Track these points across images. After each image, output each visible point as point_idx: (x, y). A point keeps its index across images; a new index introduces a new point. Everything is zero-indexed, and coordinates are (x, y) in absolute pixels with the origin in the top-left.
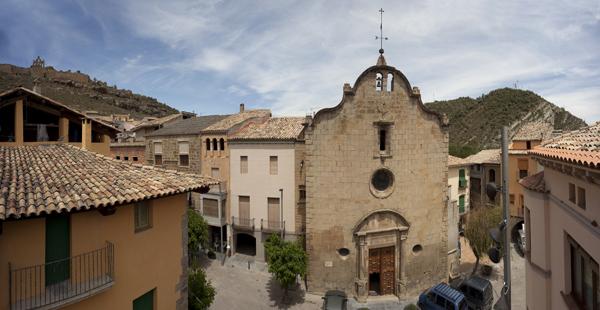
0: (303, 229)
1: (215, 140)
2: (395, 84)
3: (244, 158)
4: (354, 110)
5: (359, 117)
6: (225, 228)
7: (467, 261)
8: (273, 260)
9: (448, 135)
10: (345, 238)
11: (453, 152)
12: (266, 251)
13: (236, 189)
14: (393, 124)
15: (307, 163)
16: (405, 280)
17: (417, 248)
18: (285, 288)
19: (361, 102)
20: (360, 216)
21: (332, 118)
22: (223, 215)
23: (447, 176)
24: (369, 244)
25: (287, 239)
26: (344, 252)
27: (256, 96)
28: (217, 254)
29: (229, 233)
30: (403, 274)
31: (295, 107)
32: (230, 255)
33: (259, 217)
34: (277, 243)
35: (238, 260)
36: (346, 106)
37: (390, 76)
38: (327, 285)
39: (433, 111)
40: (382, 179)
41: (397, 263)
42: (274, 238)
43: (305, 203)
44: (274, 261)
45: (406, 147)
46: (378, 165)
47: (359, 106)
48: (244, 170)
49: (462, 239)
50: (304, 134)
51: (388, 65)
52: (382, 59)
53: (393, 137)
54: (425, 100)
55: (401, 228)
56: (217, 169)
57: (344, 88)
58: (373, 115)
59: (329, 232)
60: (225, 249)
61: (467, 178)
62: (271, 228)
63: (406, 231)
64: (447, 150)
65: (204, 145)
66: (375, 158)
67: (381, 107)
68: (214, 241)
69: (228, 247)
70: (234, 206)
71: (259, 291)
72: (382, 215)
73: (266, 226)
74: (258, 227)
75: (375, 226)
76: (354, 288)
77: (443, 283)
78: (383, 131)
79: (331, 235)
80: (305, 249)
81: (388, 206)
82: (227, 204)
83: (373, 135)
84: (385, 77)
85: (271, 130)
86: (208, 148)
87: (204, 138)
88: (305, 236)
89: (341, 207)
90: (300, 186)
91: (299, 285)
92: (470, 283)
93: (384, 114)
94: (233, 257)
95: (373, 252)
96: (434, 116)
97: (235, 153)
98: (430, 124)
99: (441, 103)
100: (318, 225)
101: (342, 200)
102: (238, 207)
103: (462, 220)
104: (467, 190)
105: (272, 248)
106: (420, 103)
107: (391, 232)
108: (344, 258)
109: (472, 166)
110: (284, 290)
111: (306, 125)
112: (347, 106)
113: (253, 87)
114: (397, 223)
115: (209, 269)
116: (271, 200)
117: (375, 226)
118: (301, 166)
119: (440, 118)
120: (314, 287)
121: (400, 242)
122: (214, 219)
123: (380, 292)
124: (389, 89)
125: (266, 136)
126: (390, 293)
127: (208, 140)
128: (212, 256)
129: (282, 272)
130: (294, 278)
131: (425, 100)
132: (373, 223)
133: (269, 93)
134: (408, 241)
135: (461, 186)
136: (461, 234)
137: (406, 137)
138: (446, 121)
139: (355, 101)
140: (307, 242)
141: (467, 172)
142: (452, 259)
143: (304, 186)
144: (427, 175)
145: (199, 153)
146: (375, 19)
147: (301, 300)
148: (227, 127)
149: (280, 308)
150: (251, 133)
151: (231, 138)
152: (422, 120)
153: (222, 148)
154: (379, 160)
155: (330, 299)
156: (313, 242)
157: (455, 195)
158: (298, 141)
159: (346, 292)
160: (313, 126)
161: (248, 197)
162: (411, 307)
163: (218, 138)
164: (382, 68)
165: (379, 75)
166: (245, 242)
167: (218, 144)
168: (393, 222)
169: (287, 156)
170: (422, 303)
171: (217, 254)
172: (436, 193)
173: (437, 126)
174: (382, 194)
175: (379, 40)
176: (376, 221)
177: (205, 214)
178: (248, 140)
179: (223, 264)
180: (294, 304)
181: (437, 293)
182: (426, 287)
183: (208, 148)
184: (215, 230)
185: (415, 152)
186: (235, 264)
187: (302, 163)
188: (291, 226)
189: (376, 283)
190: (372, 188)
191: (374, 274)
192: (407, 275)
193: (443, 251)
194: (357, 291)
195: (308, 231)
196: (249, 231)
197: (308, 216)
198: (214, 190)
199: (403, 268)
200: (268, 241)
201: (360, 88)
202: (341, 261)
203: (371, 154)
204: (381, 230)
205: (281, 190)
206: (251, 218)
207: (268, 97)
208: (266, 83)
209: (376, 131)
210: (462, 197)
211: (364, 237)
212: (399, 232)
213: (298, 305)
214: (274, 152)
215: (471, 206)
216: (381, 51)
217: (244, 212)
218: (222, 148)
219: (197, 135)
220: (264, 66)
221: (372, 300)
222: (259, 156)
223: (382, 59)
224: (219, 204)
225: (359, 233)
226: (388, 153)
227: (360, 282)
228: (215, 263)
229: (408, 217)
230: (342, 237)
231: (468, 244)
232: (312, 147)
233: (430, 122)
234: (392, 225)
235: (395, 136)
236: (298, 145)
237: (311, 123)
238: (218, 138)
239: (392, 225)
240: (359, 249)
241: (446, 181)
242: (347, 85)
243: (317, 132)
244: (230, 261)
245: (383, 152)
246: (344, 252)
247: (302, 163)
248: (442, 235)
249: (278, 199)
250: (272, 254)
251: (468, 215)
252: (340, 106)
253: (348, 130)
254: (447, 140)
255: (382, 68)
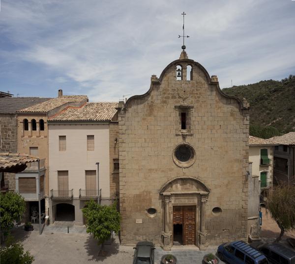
0: (117, 194)
1: (34, 122)
2: (194, 74)
3: (62, 138)
4: (160, 97)
5: (165, 102)
6: (43, 201)
7: (268, 228)
8: (89, 222)
9: (248, 118)
10: (152, 200)
11: (253, 133)
12: (84, 216)
13: (54, 165)
14: (193, 107)
15: (120, 140)
16: (205, 233)
17: (217, 210)
18: (102, 245)
19: (166, 90)
20: (165, 181)
21: (141, 104)
22: (42, 189)
23: (247, 153)
24: (173, 202)
25: (103, 204)
26: (152, 211)
27: (74, 84)
28: (35, 225)
29: (48, 205)
30: (203, 228)
31: (110, 93)
32: (48, 224)
33: (77, 187)
34: (94, 208)
35: (57, 227)
36: (153, 93)
37: (189, 68)
38: (138, 238)
39: (233, 96)
40: (184, 153)
41: (198, 219)
42: (91, 203)
43: (118, 174)
44: (91, 222)
45: (205, 127)
46: (180, 141)
47: (164, 93)
48: (62, 148)
49: (263, 210)
50: (117, 117)
51: (189, 58)
52: (184, 53)
53: (193, 119)
54: (222, 86)
55: (202, 192)
56: (37, 148)
57: (152, 78)
58: (175, 100)
59: (139, 196)
60: (44, 219)
61: (270, 157)
62: (89, 196)
63: (206, 196)
64: (248, 131)
65: (21, 126)
66: (177, 135)
67: (181, 94)
68: (31, 214)
69: (47, 217)
70: (53, 183)
71: (78, 250)
72: (184, 181)
73: (83, 195)
74: (76, 196)
75: (178, 189)
76: (160, 239)
77: (242, 242)
78: (184, 115)
79: (141, 198)
80: (119, 211)
81: (189, 174)
82: (45, 179)
83: (176, 116)
84: (184, 68)
85: (88, 113)
86: (26, 128)
87: (21, 119)
88: (118, 199)
89: (150, 171)
90: (114, 160)
91: (113, 240)
92: (272, 248)
93: (184, 100)
94: (51, 225)
95: (176, 209)
96: (232, 101)
97: (53, 134)
98: (230, 108)
99: (240, 87)
100: (130, 189)
101: (150, 170)
102: (56, 180)
103: (264, 193)
104: (270, 169)
105: (89, 213)
106: (218, 89)
107: (192, 194)
108: (152, 216)
109: (276, 147)
110: (101, 245)
111: (119, 109)
112: (153, 93)
113: (71, 75)
114: (197, 188)
115: (26, 241)
116: (88, 172)
117: (178, 189)
118: (115, 143)
119: (239, 103)
120: (128, 240)
121: (201, 204)
122: (31, 195)
123: (182, 243)
124: (188, 78)
125: (84, 118)
126: (191, 244)
127: (26, 122)
128: (28, 228)
129: (99, 231)
130: (110, 235)
131: (222, 86)
132: (177, 187)
133: (87, 81)
134: (208, 203)
135: (263, 163)
136: (263, 206)
137: (205, 119)
138: (246, 105)
139: (161, 90)
140: (121, 205)
141: (269, 151)
142: (252, 224)
143: (118, 160)
144: (227, 152)
145: (15, 133)
146: (178, 21)
147: (115, 252)
148: (48, 109)
149: (97, 260)
150: (69, 115)
151: (52, 119)
152: (221, 104)
153: (42, 128)
154: (181, 137)
155: (140, 249)
156: (125, 205)
157: (256, 170)
158: (113, 122)
159: (154, 243)
160: (125, 110)
161: (67, 171)
162: (209, 257)
163: (37, 119)
164: (184, 61)
165: (179, 67)
166: (64, 210)
167: (38, 125)
168: (194, 187)
169: (103, 135)
170: (222, 253)
171: (35, 225)
172: (236, 167)
173: (237, 110)
174: (184, 164)
175: (182, 38)
176: (178, 185)
177: (20, 192)
178: (67, 121)
179: (41, 233)
180: (109, 255)
181: (236, 248)
182: (225, 241)
183: (26, 128)
184: (32, 205)
185: (214, 131)
186: (55, 232)
187: (116, 140)
188: (106, 192)
189: (179, 234)
190: (177, 162)
191: (178, 224)
192: (207, 229)
193: (243, 215)
194: (163, 241)
195: (121, 196)
196: (69, 201)
197: (121, 183)
198: (33, 167)
199: (204, 223)
200: (86, 206)
201: (165, 78)
202: (150, 218)
203: (174, 132)
204: (183, 192)
205: (98, 164)
206: (70, 189)
207: (84, 85)
208: (83, 73)
209: (178, 113)
210: (264, 174)
211: (169, 197)
212: (200, 196)
213: (113, 255)
214: (91, 132)
215: (275, 182)
216: (184, 48)
217: (63, 185)
218: (42, 128)
219: (12, 115)
220: (81, 58)
221: (175, 249)
222: (76, 136)
223: (184, 53)
224: (37, 181)
225: (164, 193)
226: (189, 131)
227: (165, 235)
228: (34, 234)
229: (208, 184)
230: (150, 200)
231: (269, 215)
232: (124, 128)
233: (229, 106)
234: (194, 190)
235: (194, 117)
236: (112, 126)
237: (123, 107)
238: (37, 119)
239: (194, 190)
240: (164, 208)
241: (246, 158)
242: (154, 77)
243: (128, 115)
244: (49, 229)
245: (184, 131)
246: (152, 211)
247: (116, 140)
248: (243, 203)
249: (95, 171)
250: (89, 218)
251: (272, 191)
252: (148, 94)
253: (155, 113)
254: (248, 122)
255: (184, 61)
